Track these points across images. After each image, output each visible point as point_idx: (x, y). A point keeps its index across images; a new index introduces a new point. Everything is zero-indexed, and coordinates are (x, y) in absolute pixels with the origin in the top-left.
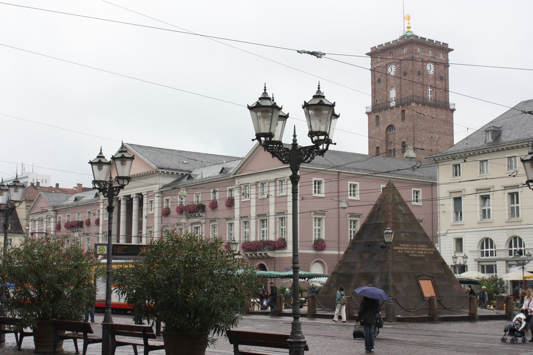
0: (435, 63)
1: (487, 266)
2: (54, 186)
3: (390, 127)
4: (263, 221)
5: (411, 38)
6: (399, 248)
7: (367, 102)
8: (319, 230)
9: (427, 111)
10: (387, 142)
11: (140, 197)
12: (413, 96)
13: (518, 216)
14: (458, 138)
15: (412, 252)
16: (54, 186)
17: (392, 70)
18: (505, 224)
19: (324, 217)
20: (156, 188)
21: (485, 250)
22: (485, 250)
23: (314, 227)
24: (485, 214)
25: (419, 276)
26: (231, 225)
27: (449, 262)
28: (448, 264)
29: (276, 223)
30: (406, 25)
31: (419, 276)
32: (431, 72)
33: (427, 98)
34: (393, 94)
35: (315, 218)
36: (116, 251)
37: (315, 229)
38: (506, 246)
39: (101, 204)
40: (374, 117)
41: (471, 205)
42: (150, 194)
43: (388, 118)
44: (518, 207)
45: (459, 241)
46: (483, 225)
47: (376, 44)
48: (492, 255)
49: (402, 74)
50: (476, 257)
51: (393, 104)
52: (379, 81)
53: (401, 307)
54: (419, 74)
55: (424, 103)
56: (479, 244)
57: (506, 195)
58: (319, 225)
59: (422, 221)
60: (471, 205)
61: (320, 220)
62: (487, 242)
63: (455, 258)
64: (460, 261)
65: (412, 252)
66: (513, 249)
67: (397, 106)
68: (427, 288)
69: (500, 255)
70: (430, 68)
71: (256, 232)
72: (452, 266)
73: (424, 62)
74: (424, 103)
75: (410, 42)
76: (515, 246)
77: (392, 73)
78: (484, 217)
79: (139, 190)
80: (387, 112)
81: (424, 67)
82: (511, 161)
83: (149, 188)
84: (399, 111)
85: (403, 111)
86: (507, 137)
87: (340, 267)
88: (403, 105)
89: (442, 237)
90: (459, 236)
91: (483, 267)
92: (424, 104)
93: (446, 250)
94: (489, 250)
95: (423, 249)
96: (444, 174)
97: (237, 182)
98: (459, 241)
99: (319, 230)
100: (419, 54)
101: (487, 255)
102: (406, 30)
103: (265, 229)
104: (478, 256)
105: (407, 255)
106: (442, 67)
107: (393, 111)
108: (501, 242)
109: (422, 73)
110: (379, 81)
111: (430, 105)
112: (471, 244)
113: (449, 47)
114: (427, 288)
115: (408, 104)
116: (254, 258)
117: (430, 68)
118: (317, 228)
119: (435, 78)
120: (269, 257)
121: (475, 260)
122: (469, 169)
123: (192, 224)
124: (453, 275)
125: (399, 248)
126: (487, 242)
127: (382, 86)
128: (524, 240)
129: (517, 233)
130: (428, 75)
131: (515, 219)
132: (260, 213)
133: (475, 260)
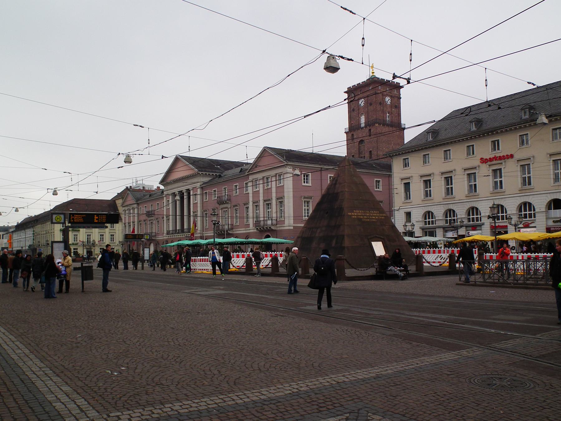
0: (391, 97)
1: (429, 232)
2: (142, 188)
3: (361, 142)
4: (268, 204)
5: (375, 79)
6: (353, 214)
7: (345, 125)
8: (308, 210)
9: (386, 129)
10: (359, 151)
11: (188, 191)
12: (376, 119)
13: (452, 194)
14: (406, 141)
15: (365, 217)
16: (142, 188)
17: (362, 102)
18: (442, 200)
19: (311, 200)
20: (198, 185)
21: (427, 220)
22: (427, 220)
23: (304, 208)
24: (428, 194)
25: (371, 238)
26: (247, 208)
27: (401, 229)
28: (400, 231)
29: (277, 205)
30: (371, 71)
31: (371, 238)
32: (389, 103)
33: (386, 121)
34: (363, 120)
35: (305, 202)
36: (73, 219)
37: (305, 209)
38: (443, 216)
39: (165, 198)
40: (350, 135)
41: (417, 188)
42: (195, 189)
43: (359, 134)
44: (452, 188)
45: (408, 214)
46: (426, 202)
47: (351, 85)
48: (433, 224)
49: (369, 104)
50: (421, 226)
51: (363, 125)
52: (353, 110)
53: (350, 264)
54: (380, 104)
55: (384, 124)
56: (423, 216)
57: (443, 179)
58: (308, 206)
59: (382, 202)
60: (417, 188)
61: (308, 202)
62: (428, 215)
63: (405, 226)
64: (409, 228)
65: (365, 217)
66: (448, 218)
67: (366, 127)
68: (379, 249)
69: (439, 224)
70: (388, 99)
71: (264, 212)
72: (403, 232)
73: (384, 96)
74: (384, 124)
75: (374, 83)
76: (450, 217)
77: (362, 104)
78: (427, 196)
79: (187, 187)
80: (359, 131)
81: (384, 99)
82: (447, 154)
83: (194, 185)
84: (367, 130)
85: (370, 130)
86: (443, 136)
87: (303, 232)
88: (370, 126)
89: (396, 212)
90: (408, 210)
91: (426, 232)
92: (384, 125)
93: (399, 221)
94: (431, 220)
95: (374, 215)
96: (397, 165)
97: (251, 178)
98: (408, 214)
99: (308, 210)
100: (380, 90)
101: (429, 224)
102: (371, 74)
103: (270, 210)
104: (422, 225)
105: (360, 220)
106: (396, 99)
107: (363, 131)
108: (439, 213)
109: (383, 103)
110: (353, 110)
111: (388, 125)
112: (417, 216)
113: (401, 85)
114: (379, 249)
115: (373, 124)
116: (263, 231)
117: (388, 99)
118: (306, 208)
119: (391, 106)
120: (273, 230)
121: (420, 228)
122: (415, 160)
123: (222, 209)
124: (402, 237)
125: (353, 214)
126: (428, 215)
127: (354, 114)
128: (457, 212)
129: (451, 207)
130: (386, 104)
131: (450, 196)
132: (266, 198)
133: (420, 228)
